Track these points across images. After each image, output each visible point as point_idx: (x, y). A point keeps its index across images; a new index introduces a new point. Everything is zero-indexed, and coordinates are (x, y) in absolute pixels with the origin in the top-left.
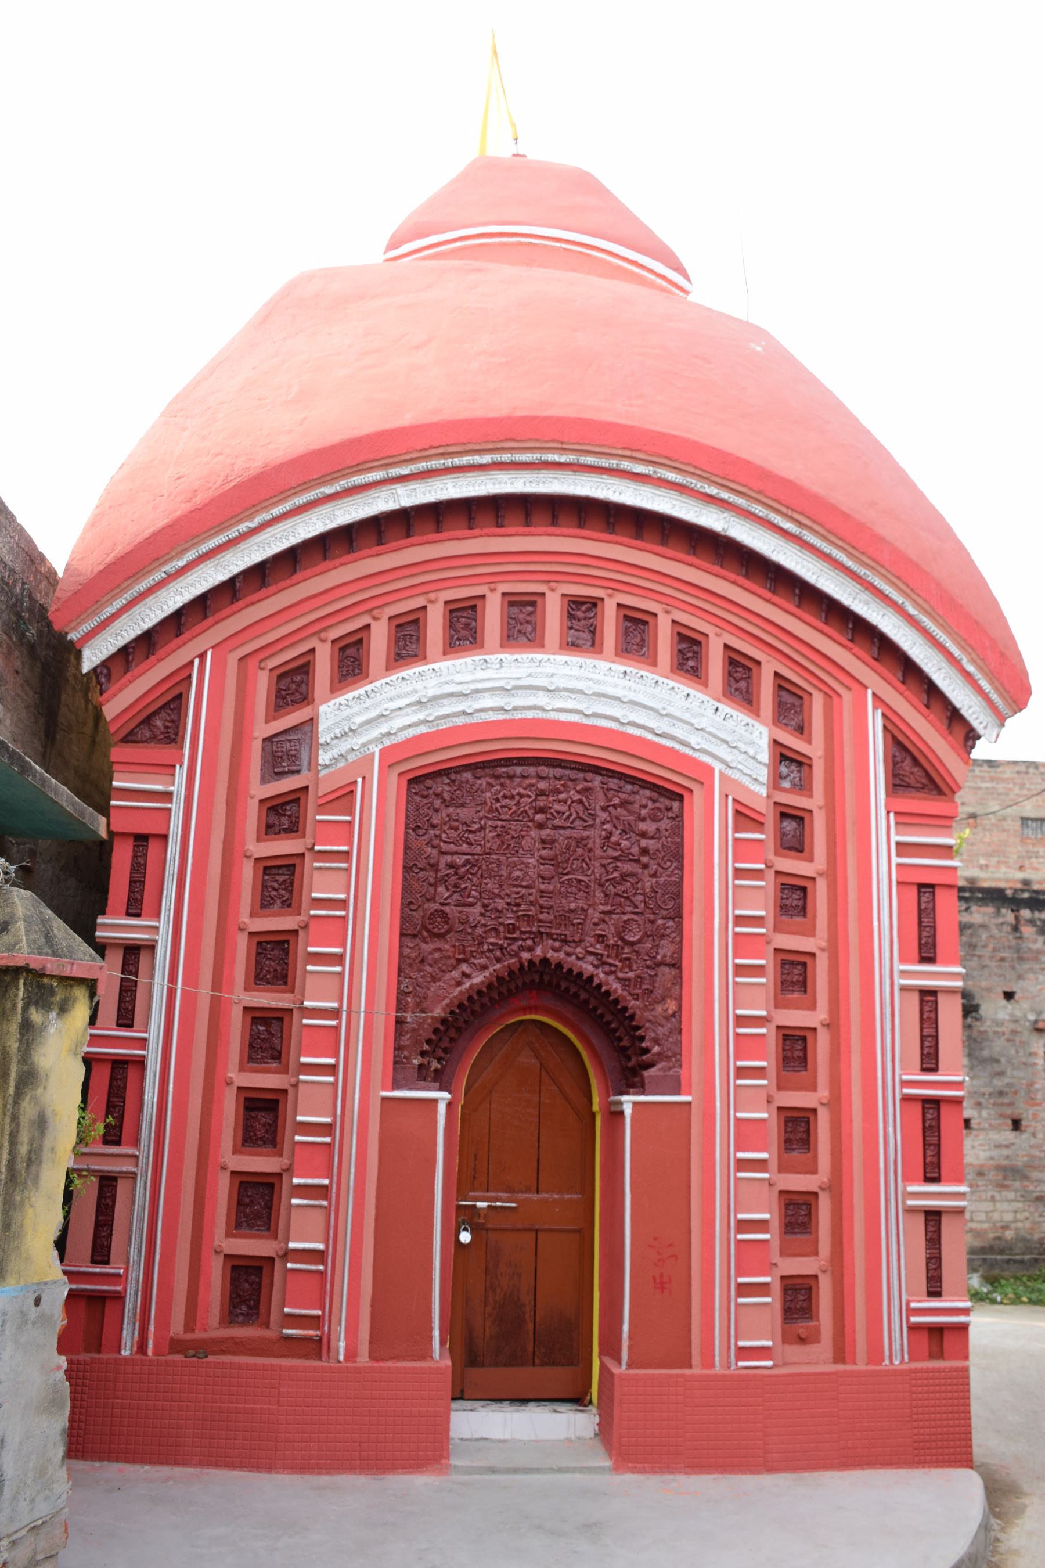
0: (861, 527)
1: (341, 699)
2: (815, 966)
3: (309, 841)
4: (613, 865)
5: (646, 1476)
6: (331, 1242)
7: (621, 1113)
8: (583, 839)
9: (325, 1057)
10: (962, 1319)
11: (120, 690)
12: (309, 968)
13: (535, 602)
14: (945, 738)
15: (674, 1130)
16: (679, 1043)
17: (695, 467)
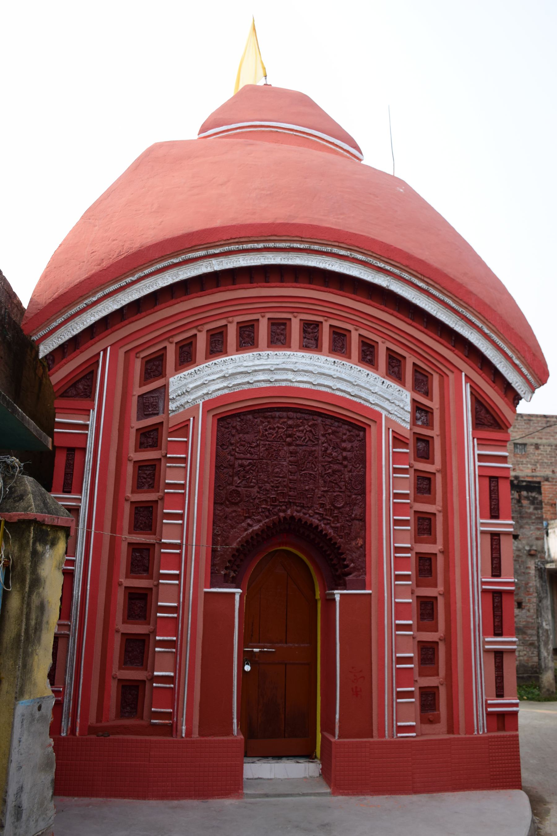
0: (461, 286)
1: (182, 375)
2: (436, 520)
3: (164, 452)
4: (328, 466)
5: (350, 797)
6: (177, 671)
7: (334, 600)
8: (312, 451)
9: (174, 570)
10: (515, 709)
11: (60, 368)
12: (164, 521)
13: (286, 323)
14: (503, 399)
15: (361, 609)
16: (364, 562)
17: (372, 252)
